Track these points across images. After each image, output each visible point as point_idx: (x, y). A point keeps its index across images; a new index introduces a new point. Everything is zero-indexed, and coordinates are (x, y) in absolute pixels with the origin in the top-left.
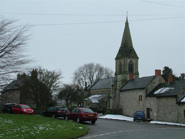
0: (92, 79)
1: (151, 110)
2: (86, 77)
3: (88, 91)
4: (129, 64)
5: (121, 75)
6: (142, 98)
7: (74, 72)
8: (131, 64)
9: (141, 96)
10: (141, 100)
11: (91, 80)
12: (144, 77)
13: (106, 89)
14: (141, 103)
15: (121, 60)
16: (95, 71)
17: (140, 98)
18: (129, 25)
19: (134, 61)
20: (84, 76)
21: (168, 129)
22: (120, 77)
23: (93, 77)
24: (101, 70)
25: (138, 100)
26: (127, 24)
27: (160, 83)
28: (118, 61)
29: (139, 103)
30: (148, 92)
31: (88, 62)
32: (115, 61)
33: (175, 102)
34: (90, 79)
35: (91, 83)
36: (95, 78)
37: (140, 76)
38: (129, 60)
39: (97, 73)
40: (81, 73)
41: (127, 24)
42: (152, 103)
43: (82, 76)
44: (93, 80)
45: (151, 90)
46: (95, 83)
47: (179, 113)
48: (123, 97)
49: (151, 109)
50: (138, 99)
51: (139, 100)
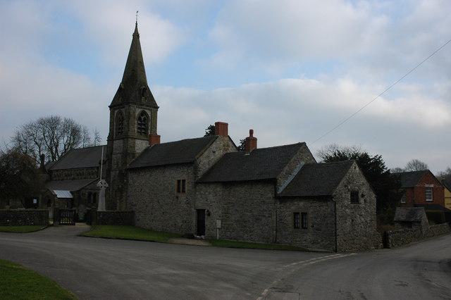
0: (54, 150)
1: (209, 215)
2: (43, 147)
3: (52, 174)
4: (140, 119)
5: (122, 141)
6: (179, 188)
7: (15, 135)
8: (142, 118)
9: (184, 181)
10: (184, 191)
11: (52, 153)
12: (186, 140)
13: (87, 168)
14: (183, 197)
15: (123, 110)
16: (62, 135)
17: (181, 186)
18: (141, 40)
19: (149, 113)
20: (36, 143)
21: (352, 256)
22: (118, 144)
23: (57, 146)
24: (75, 132)
25: (176, 192)
26: (136, 36)
27: (227, 154)
28: (116, 111)
29: (177, 197)
30: (200, 174)
31: (47, 114)
32: (108, 111)
33: (270, 195)
34: (51, 149)
35: (54, 158)
36: (61, 148)
37: (161, 143)
38: (138, 111)
39: (66, 138)
40: (32, 137)
41: (136, 36)
42: (211, 197)
43: (33, 144)
44: (57, 150)
45: (207, 167)
46: (60, 158)
47: (281, 220)
48: (137, 184)
49: (208, 211)
50: (176, 188)
51: (179, 191)
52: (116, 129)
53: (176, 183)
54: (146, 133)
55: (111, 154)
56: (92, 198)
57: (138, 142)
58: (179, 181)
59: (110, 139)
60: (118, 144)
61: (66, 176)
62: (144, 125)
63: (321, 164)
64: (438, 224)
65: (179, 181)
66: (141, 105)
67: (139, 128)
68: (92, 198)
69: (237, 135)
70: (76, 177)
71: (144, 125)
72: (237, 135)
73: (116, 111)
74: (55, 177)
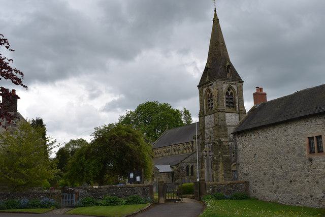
4: (227, 93)
8: (229, 93)
18: (221, 23)
19: (235, 87)
22: (209, 119)
25: (306, 153)
26: (216, 21)
28: (205, 90)
41: (216, 21)
50: (307, 147)
51: (311, 151)
52: (235, 102)
53: (306, 142)
54: (234, 107)
55: (204, 128)
56: (190, 170)
57: (227, 115)
58: (310, 139)
59: (202, 115)
60: (209, 119)
61: (156, 154)
62: (231, 99)
63: (94, 143)
64: (214, 214)
65: (310, 139)
66: (228, 80)
67: (227, 102)
68: (190, 170)
69: (35, 119)
70: (174, 153)
71: (231, 99)
72: (35, 119)
73: (205, 90)
74: (156, 154)
